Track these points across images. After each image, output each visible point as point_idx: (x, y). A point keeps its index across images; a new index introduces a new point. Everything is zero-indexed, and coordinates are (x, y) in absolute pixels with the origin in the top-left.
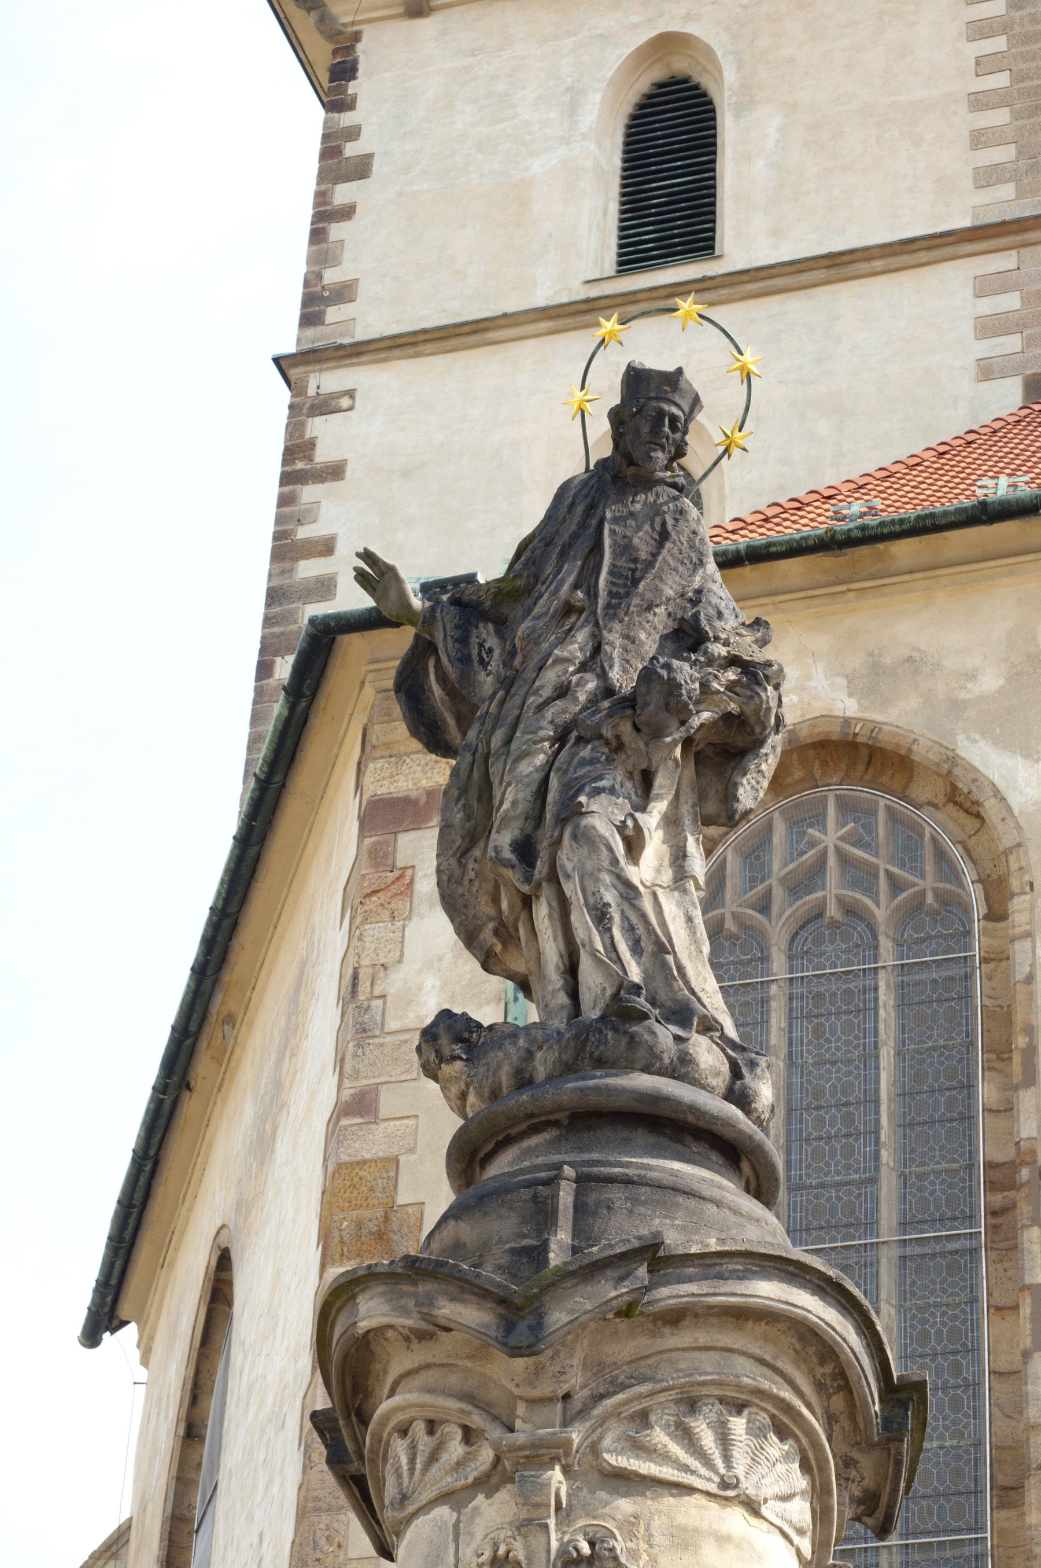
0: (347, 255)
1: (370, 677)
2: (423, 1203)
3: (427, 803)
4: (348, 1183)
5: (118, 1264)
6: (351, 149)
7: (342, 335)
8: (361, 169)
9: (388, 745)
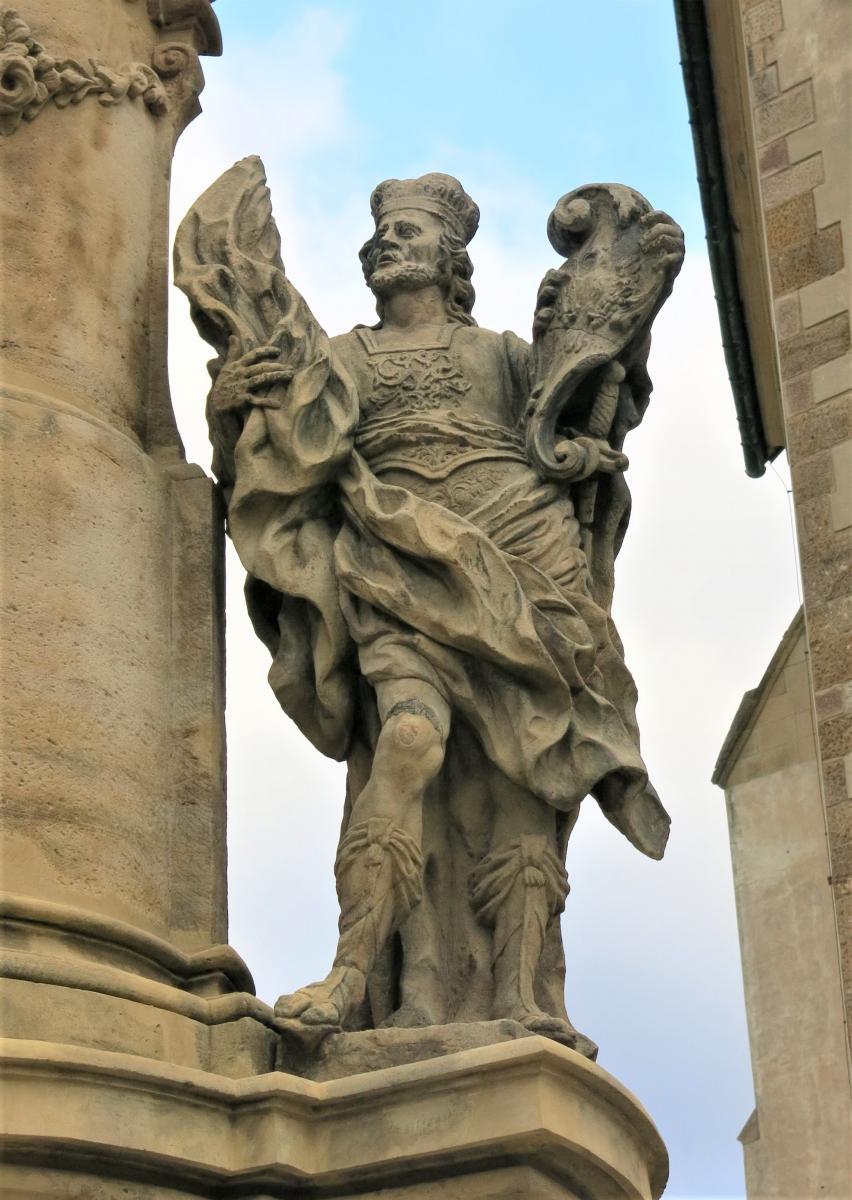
2: (839, 222)
4: (776, 225)
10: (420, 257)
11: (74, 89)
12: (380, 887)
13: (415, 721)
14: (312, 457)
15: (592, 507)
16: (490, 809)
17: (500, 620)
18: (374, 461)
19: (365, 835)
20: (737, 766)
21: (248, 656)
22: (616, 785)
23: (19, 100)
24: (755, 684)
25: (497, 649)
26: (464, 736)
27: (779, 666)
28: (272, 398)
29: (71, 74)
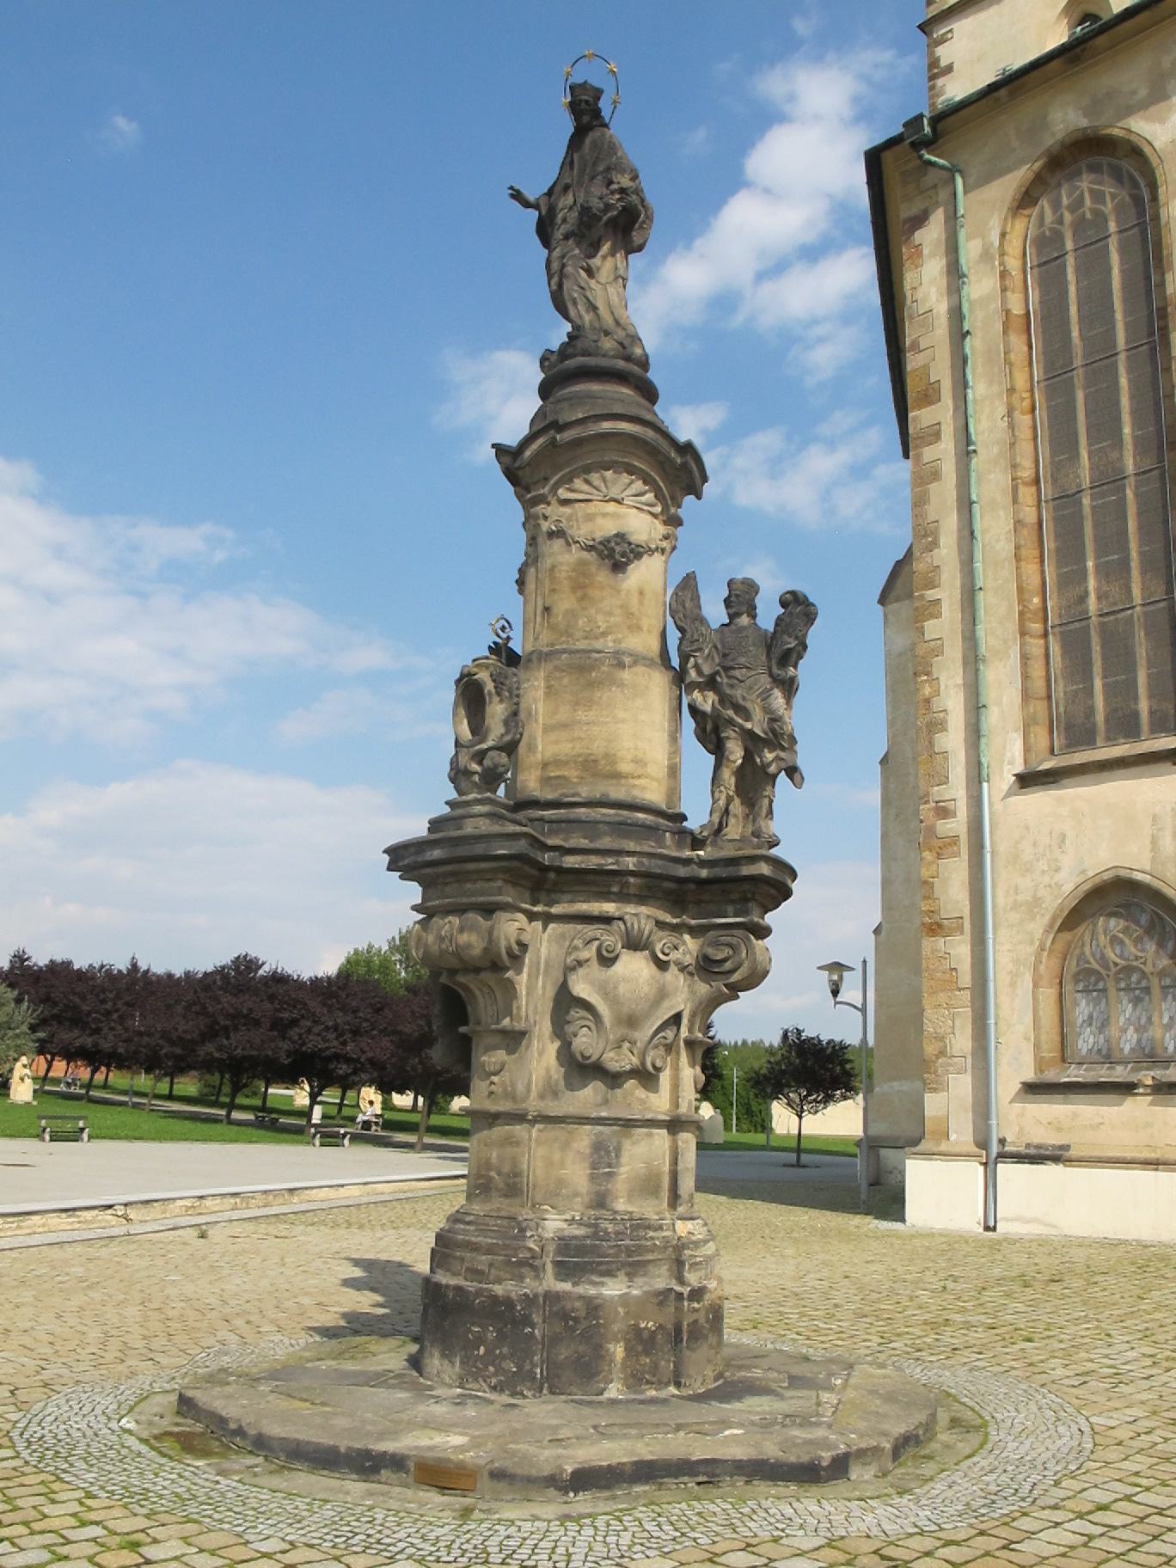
10: (741, 597)
12: (723, 797)
17: (757, 725)
21: (689, 724)
26: (748, 756)
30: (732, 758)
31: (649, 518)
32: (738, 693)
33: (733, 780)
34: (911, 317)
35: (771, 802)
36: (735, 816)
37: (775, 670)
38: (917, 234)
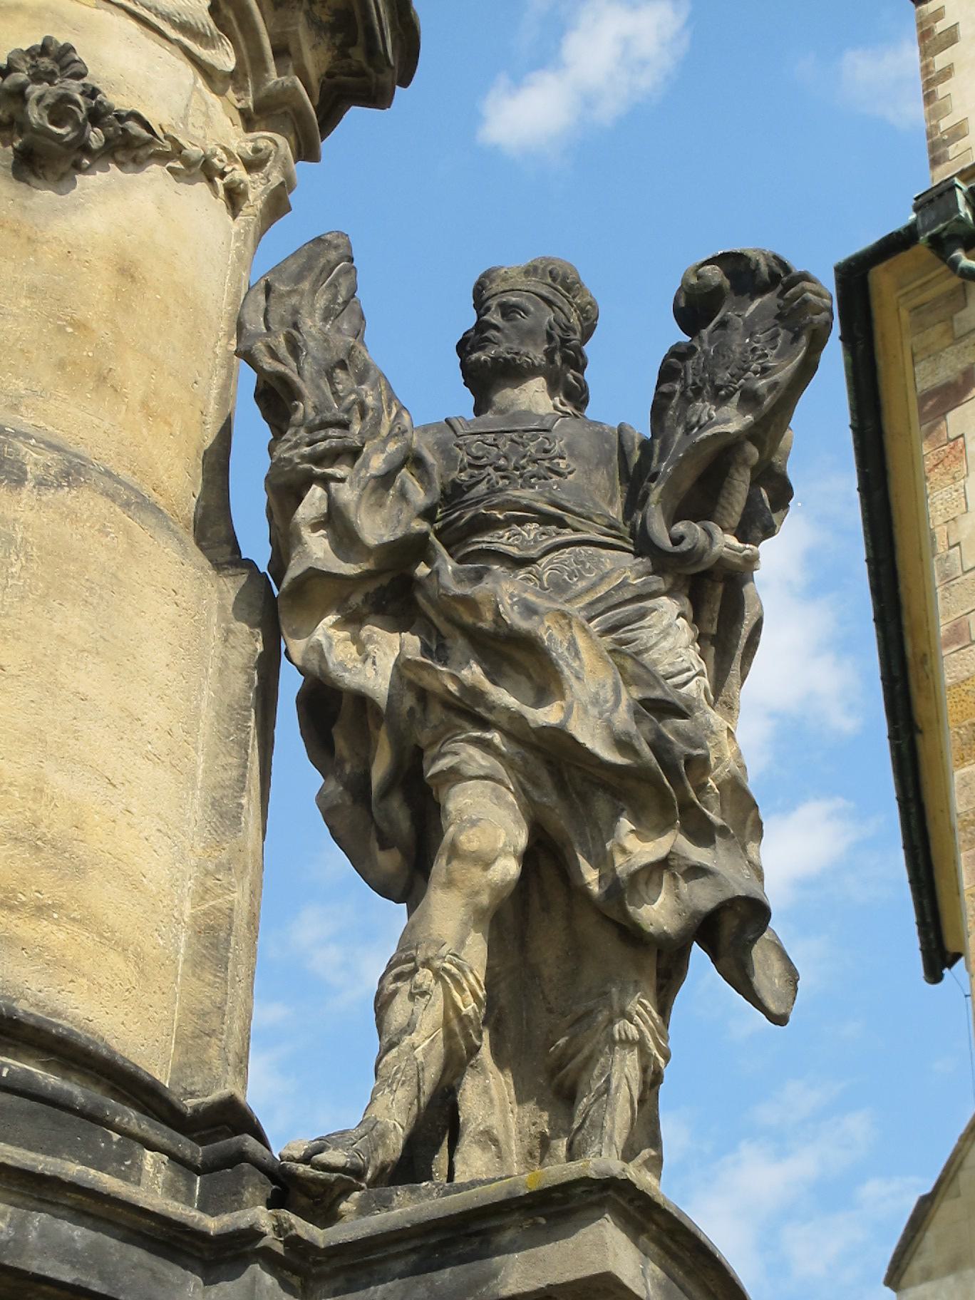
0: (955, 102)
1: (901, 301)
3: (964, 382)
5: (925, 902)
6: (940, 27)
7: (964, 163)
8: (951, 37)
9: (925, 349)
11: (137, 143)
12: (430, 1017)
13: (488, 824)
14: (376, 529)
15: (716, 615)
16: (577, 951)
17: (590, 710)
18: (454, 548)
19: (413, 959)
20: (909, 1269)
22: (730, 924)
23: (67, 139)
24: (928, 1189)
25: (589, 745)
26: (545, 856)
27: (953, 1169)
28: (339, 471)
29: (134, 128)
30: (470, 841)
31: (188, 72)
32: (506, 595)
33: (476, 952)
34: (948, 578)
35: (652, 1080)
36: (489, 1139)
37: (659, 531)
38: (951, 416)
